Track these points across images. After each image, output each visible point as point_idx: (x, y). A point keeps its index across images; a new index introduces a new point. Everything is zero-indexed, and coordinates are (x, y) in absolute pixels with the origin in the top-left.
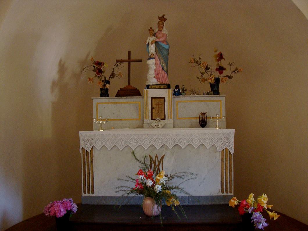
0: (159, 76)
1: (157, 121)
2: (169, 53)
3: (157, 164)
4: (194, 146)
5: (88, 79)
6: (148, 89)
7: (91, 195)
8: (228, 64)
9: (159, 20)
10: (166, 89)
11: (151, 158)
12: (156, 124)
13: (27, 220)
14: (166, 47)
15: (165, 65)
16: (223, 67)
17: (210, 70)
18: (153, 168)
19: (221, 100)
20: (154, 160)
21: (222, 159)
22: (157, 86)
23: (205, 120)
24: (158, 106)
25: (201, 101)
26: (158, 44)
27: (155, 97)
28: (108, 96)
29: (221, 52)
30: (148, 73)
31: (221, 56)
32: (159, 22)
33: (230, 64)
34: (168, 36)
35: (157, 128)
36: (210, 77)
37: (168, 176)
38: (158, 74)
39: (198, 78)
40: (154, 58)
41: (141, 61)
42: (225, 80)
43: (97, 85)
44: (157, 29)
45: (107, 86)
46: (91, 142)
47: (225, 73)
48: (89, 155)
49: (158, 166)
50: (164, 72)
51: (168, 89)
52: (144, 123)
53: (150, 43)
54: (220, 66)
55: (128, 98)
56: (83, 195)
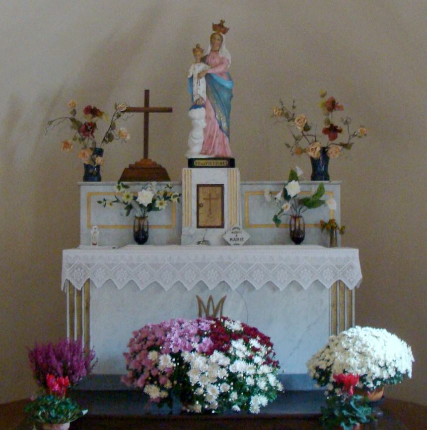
0: (212, 141)
1: (234, 231)
4: (229, 284)
6: (192, 169)
10: (226, 169)
11: (200, 302)
12: (233, 236)
14: (228, 85)
15: (225, 120)
16: (337, 127)
17: (310, 132)
20: (206, 304)
21: (334, 305)
22: (210, 161)
23: (302, 229)
28: (99, 180)
29: (332, 98)
30: (190, 135)
31: (332, 106)
32: (214, 34)
35: (235, 244)
36: (312, 147)
38: (211, 137)
39: (288, 146)
40: (204, 106)
41: (170, 110)
44: (210, 48)
45: (99, 160)
46: (85, 271)
47: (342, 138)
48: (83, 296)
50: (222, 133)
51: (229, 169)
52: (183, 233)
53: (195, 76)
54: (332, 125)
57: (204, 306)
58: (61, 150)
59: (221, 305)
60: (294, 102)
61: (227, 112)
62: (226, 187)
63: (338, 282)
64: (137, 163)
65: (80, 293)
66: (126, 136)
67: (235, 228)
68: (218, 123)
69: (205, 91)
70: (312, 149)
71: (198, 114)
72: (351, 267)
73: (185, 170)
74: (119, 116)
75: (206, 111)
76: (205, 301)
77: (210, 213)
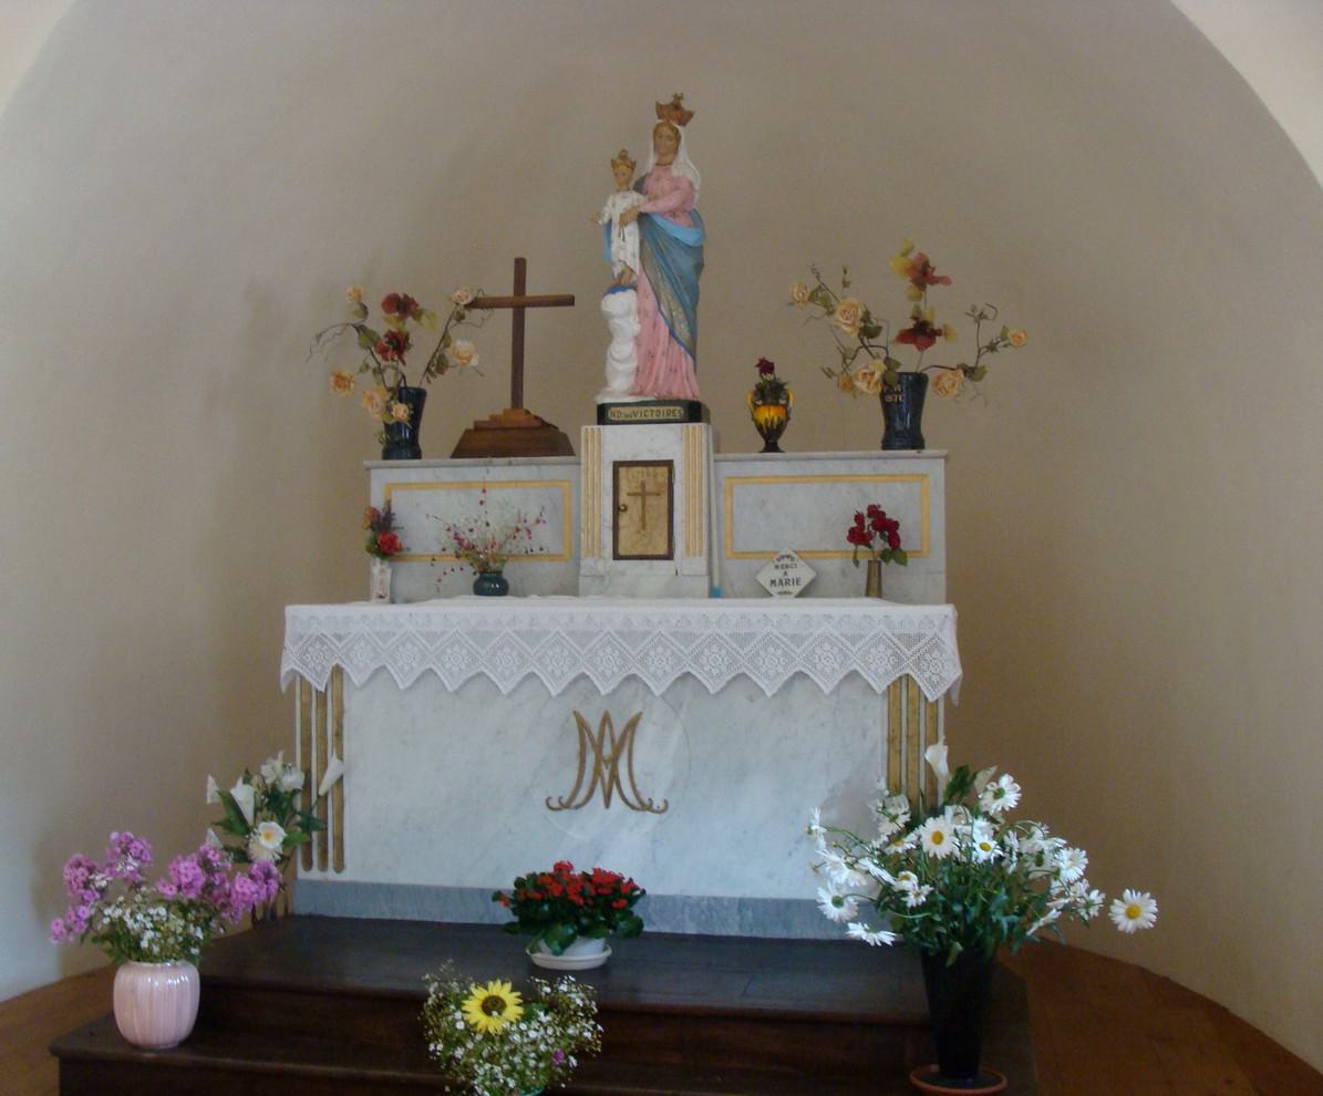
2: (699, 267)
3: (607, 751)
5: (332, 379)
6: (601, 427)
7: (331, 875)
8: (968, 314)
9: (659, 118)
11: (582, 726)
12: (777, 575)
13: (78, 978)
14: (688, 236)
15: (682, 317)
18: (592, 772)
19: (926, 476)
20: (595, 731)
21: (891, 741)
22: (643, 409)
24: (651, 494)
25: (838, 478)
26: (653, 223)
27: (629, 459)
28: (417, 454)
30: (608, 353)
32: (658, 126)
33: (977, 314)
34: (697, 188)
37: (655, 807)
39: (829, 373)
40: (634, 287)
41: (569, 301)
42: (954, 385)
43: (373, 409)
44: (652, 159)
46: (785, 653)
48: (328, 702)
49: (614, 760)
52: (582, 572)
53: (616, 220)
55: (518, 465)
56: (302, 874)
57: (592, 739)
58: (332, 391)
59: (629, 734)
60: (845, 272)
61: (687, 299)
62: (675, 464)
63: (904, 682)
64: (494, 419)
65: (322, 697)
66: (469, 359)
67: (783, 557)
68: (667, 323)
69: (637, 255)
70: (865, 374)
71: (620, 306)
72: (936, 644)
73: (587, 429)
74: (460, 318)
75: (638, 296)
76: (594, 724)
77: (644, 527)
